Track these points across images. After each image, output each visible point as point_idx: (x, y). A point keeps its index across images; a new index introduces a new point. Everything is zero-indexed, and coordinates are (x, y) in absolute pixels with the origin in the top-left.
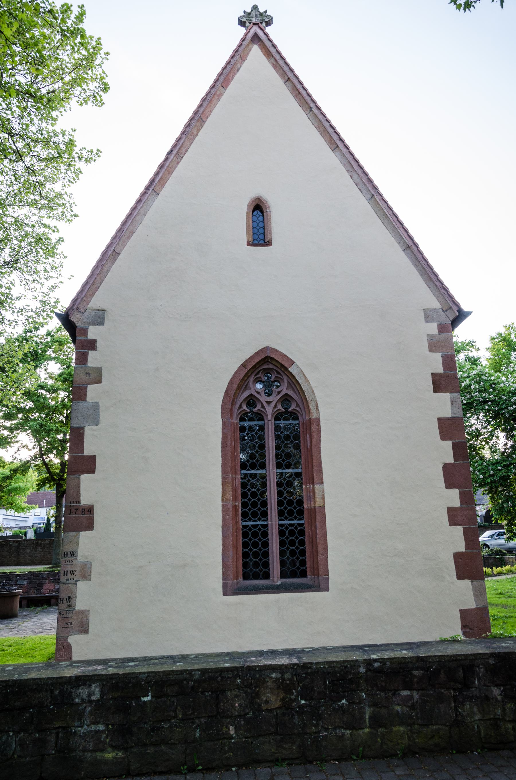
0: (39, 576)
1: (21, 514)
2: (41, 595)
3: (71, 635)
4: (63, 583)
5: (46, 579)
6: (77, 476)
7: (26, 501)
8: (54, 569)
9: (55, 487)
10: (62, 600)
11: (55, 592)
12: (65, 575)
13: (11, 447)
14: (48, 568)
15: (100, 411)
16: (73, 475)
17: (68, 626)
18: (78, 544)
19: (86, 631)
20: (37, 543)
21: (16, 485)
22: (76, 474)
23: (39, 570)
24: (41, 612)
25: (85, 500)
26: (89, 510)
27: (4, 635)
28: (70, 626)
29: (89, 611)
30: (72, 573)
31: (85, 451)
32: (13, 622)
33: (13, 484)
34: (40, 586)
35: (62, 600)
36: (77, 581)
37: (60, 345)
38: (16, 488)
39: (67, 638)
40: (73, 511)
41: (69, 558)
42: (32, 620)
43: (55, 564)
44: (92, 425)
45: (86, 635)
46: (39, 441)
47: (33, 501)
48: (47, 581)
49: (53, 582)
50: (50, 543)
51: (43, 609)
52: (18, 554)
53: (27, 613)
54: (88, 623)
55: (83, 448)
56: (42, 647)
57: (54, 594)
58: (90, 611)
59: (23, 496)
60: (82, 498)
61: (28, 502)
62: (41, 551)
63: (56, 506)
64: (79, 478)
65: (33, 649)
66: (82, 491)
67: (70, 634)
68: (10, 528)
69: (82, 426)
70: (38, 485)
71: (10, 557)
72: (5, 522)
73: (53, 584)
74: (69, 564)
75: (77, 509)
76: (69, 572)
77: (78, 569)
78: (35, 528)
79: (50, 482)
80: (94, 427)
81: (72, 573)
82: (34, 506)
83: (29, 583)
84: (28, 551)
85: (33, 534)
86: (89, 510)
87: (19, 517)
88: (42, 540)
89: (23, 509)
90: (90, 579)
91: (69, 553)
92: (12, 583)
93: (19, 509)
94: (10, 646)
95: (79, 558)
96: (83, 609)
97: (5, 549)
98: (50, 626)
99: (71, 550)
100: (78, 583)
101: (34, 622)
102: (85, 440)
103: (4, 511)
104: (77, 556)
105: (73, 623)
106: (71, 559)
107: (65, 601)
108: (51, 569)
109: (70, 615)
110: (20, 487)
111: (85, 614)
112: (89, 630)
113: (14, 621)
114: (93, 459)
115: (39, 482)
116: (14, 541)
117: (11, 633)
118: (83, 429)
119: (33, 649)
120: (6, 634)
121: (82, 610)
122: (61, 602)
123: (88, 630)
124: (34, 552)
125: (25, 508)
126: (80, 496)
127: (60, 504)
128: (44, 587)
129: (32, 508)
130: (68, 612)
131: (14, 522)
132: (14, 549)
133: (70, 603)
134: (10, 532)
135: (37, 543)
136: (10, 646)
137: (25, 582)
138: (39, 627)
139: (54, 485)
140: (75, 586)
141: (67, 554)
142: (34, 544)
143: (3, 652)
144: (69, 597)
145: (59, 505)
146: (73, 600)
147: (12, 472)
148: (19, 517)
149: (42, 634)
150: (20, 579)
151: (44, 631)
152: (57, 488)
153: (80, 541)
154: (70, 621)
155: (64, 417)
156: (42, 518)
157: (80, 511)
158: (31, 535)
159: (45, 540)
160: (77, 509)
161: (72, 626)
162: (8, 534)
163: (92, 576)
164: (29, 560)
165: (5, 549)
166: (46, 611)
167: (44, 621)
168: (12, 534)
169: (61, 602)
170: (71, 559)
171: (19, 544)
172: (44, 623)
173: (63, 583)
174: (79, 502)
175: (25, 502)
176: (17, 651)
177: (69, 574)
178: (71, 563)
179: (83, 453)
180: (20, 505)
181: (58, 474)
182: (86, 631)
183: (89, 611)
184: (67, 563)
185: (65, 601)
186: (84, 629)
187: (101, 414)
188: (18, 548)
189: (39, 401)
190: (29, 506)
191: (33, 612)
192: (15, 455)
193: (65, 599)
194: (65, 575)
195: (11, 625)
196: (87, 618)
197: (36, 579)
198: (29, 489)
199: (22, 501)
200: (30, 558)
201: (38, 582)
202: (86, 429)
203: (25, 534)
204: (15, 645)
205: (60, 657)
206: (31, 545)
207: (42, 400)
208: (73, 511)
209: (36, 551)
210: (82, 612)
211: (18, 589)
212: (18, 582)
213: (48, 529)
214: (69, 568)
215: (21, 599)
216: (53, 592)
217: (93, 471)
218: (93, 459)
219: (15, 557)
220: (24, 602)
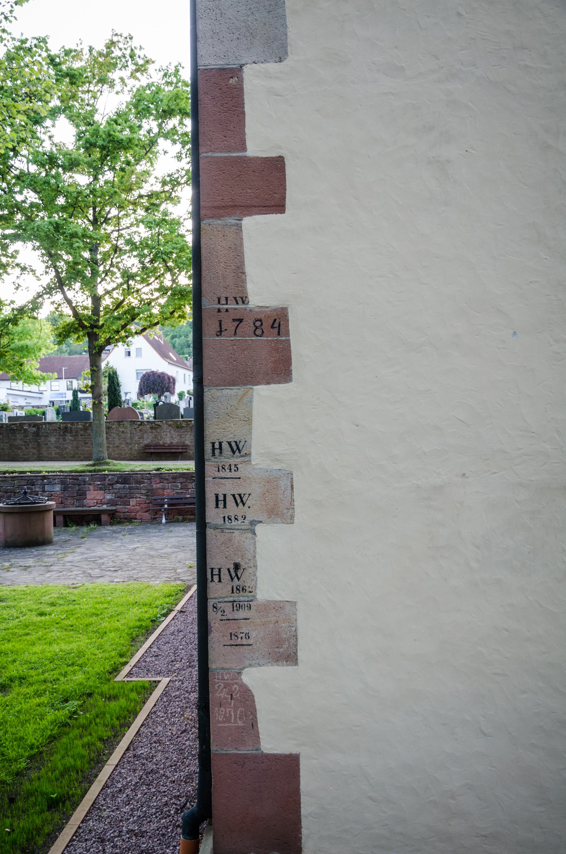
0: (78, 480)
1: (34, 388)
2: (85, 509)
3: (250, 665)
4: (216, 528)
5: (90, 484)
6: (231, 221)
7: (38, 367)
8: (97, 468)
9: (86, 339)
10: (216, 572)
11: (107, 504)
12: (221, 504)
13: (9, 274)
14: (88, 465)
15: (287, 12)
16: (219, 217)
17: (239, 641)
18: (248, 420)
19: (291, 658)
20: (66, 428)
21: (22, 343)
22: (229, 215)
23: (74, 469)
24: (88, 535)
25: (261, 295)
26: (276, 323)
27: (38, 579)
28: (244, 642)
29: (294, 604)
30: (240, 500)
31: (249, 144)
32: (48, 552)
33: (16, 341)
34: (82, 495)
35: (216, 572)
36: (253, 523)
37: (72, 83)
38: (22, 347)
39: (239, 673)
40: (229, 325)
41: (227, 459)
42: (78, 550)
43: (98, 460)
44: (266, 61)
45: (290, 668)
46: (53, 257)
47: (49, 366)
48: (91, 487)
49: (101, 489)
50: (85, 429)
51: (92, 530)
52: (39, 444)
53: (67, 538)
54: (296, 636)
55: (244, 134)
56: (111, 611)
57: (105, 507)
58: (299, 606)
59: (33, 359)
60: (250, 288)
61: (42, 369)
62: (71, 440)
63: (91, 370)
64: (239, 228)
65: (97, 615)
66: (249, 268)
67: (247, 663)
68: (22, 408)
69: (233, 63)
70: (60, 335)
71: (27, 448)
72: (11, 399)
73: (102, 492)
74: (229, 475)
75: (241, 321)
76: (230, 499)
77: (254, 491)
78: (56, 406)
79: (76, 330)
80: (272, 67)
81: (240, 500)
82: (51, 374)
83: (64, 489)
84: (53, 439)
85: (55, 415)
86: (276, 323)
87: (30, 392)
88: (72, 424)
89: (35, 378)
90: (292, 517)
91: (225, 446)
92: (37, 489)
93: (30, 379)
94: (53, 604)
95: (255, 459)
96: (278, 598)
97: (19, 436)
98: (111, 564)
99: (230, 437)
100: (258, 528)
101: (82, 554)
102: (247, 109)
103: (7, 384)
104: (248, 455)
105: (253, 634)
106: (233, 461)
107: (225, 576)
108: (92, 468)
109: (242, 614)
110: (27, 346)
111: (281, 609)
112: (299, 654)
113: (49, 550)
114: (276, 167)
115: (61, 331)
116: (30, 425)
117: (48, 575)
118: (236, 72)
119: (97, 615)
120: (41, 578)
121: (275, 602)
122: (216, 578)
123: (296, 653)
124: (61, 440)
125: (38, 378)
126: (244, 281)
127: (97, 367)
128: (88, 497)
129: (50, 378)
130: (237, 606)
131: (23, 399)
132: (31, 437)
133: (240, 583)
134: (21, 412)
135: (66, 428)
136: (53, 604)
137: (58, 488)
138: (93, 565)
139: (84, 336)
140: (250, 535)
141: (220, 448)
142: (62, 430)
143: (43, 618)
144: (237, 566)
145: (95, 368)
146: (246, 573)
147: (16, 312)
148: (30, 392)
149: (101, 580)
150: (49, 483)
151: (104, 573)
152: (90, 342)
153: (254, 412)
154: (244, 630)
155: (89, 220)
156: (62, 394)
157: (247, 326)
158: (51, 416)
159: (77, 423)
160: (241, 321)
161: (251, 641)
162: (18, 415)
163: (297, 510)
164: (56, 454)
165: (19, 436)
166: (96, 533)
167: (98, 554)
168: (24, 415)
169: (216, 578)
170: (233, 461)
171: (38, 428)
172: (101, 558)
173: (216, 528)
174: (244, 300)
175: (37, 369)
176: (67, 618)
177: (230, 501)
178: (233, 474)
179: (244, 149)
180: (31, 373)
181: (90, 317)
182: (291, 658)
183: (294, 604)
184: (222, 474)
185: (225, 576)
186: (285, 653)
187: (290, 20)
188: (37, 434)
189: (49, 183)
190: (44, 374)
191: (75, 534)
192: (18, 281)
193: (224, 572)
194: (221, 504)
195: (46, 559)
196: (292, 623)
197: (73, 484)
198: (40, 349)
199: (33, 368)
200: (58, 451)
201: (77, 488)
202: (248, 72)
203: (44, 414)
204: (61, 602)
205: (224, 722)
206: (56, 430)
207: (53, 181)
208: (229, 325)
209: (64, 440)
210: (277, 607)
211: (48, 500)
212: (47, 488)
213: (76, 408)
214: (229, 488)
215: (56, 514)
216: (103, 504)
217: (279, 207)
218: (276, 167)
219: (35, 448)
220: (60, 519)
